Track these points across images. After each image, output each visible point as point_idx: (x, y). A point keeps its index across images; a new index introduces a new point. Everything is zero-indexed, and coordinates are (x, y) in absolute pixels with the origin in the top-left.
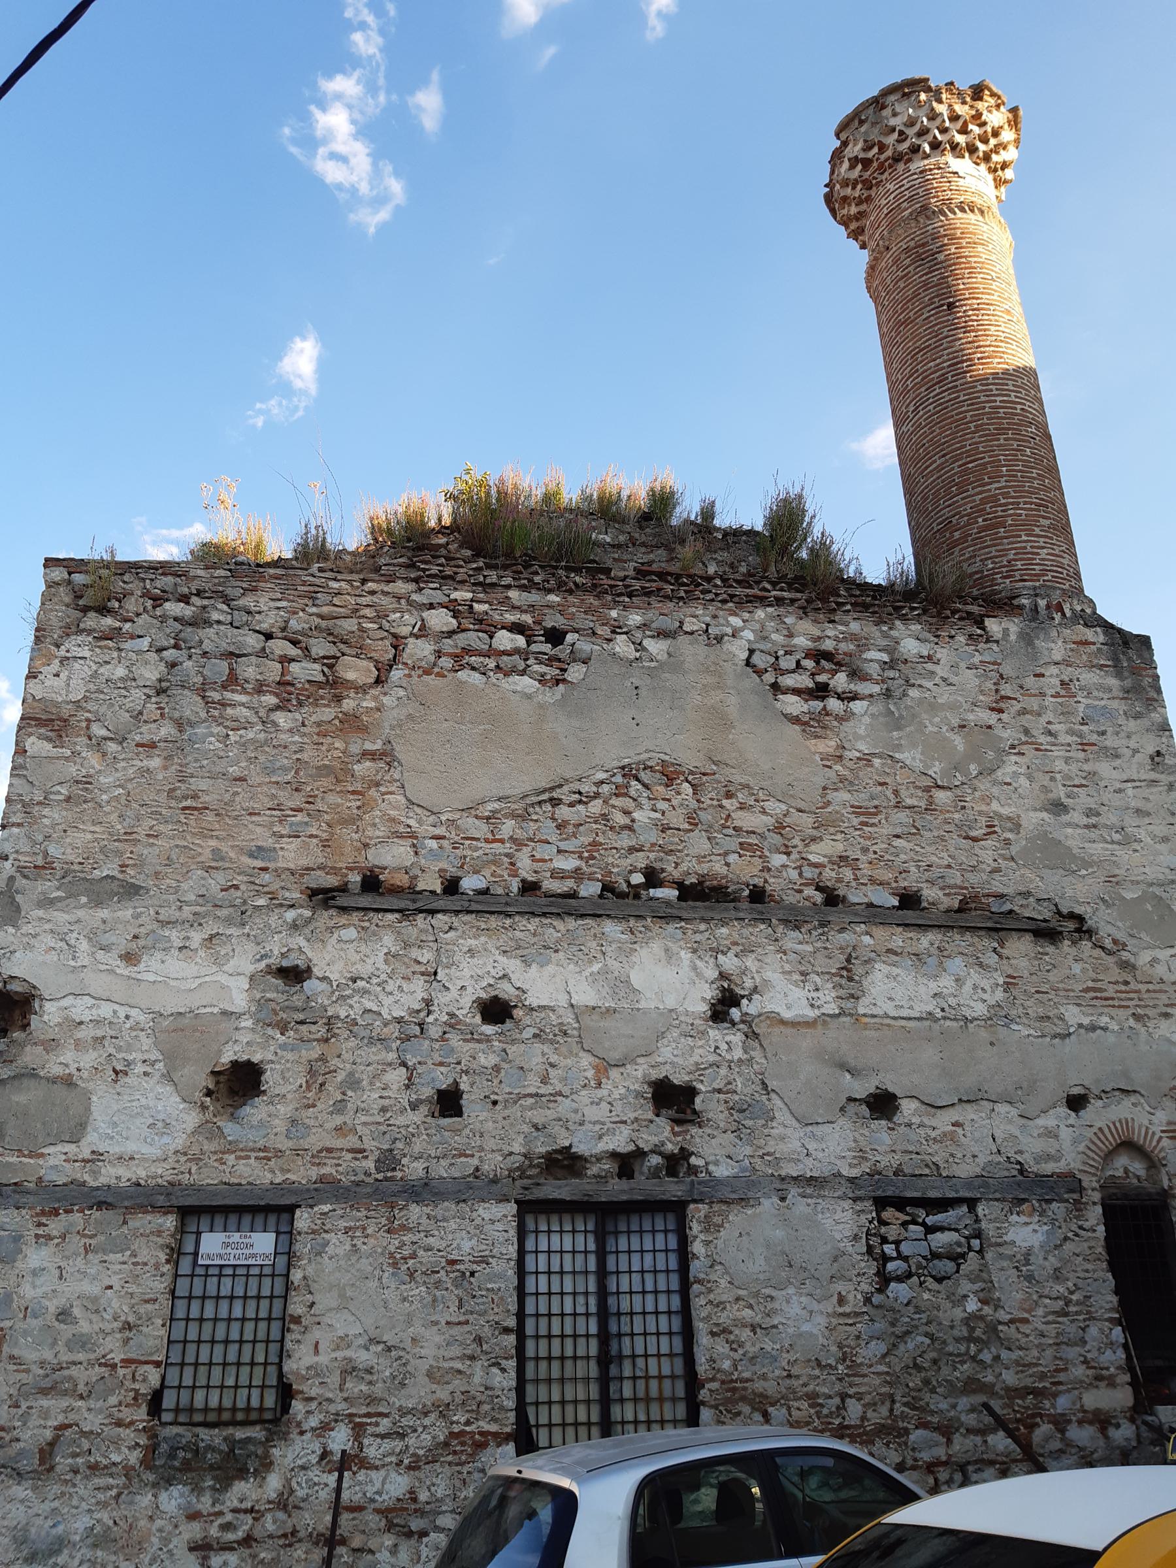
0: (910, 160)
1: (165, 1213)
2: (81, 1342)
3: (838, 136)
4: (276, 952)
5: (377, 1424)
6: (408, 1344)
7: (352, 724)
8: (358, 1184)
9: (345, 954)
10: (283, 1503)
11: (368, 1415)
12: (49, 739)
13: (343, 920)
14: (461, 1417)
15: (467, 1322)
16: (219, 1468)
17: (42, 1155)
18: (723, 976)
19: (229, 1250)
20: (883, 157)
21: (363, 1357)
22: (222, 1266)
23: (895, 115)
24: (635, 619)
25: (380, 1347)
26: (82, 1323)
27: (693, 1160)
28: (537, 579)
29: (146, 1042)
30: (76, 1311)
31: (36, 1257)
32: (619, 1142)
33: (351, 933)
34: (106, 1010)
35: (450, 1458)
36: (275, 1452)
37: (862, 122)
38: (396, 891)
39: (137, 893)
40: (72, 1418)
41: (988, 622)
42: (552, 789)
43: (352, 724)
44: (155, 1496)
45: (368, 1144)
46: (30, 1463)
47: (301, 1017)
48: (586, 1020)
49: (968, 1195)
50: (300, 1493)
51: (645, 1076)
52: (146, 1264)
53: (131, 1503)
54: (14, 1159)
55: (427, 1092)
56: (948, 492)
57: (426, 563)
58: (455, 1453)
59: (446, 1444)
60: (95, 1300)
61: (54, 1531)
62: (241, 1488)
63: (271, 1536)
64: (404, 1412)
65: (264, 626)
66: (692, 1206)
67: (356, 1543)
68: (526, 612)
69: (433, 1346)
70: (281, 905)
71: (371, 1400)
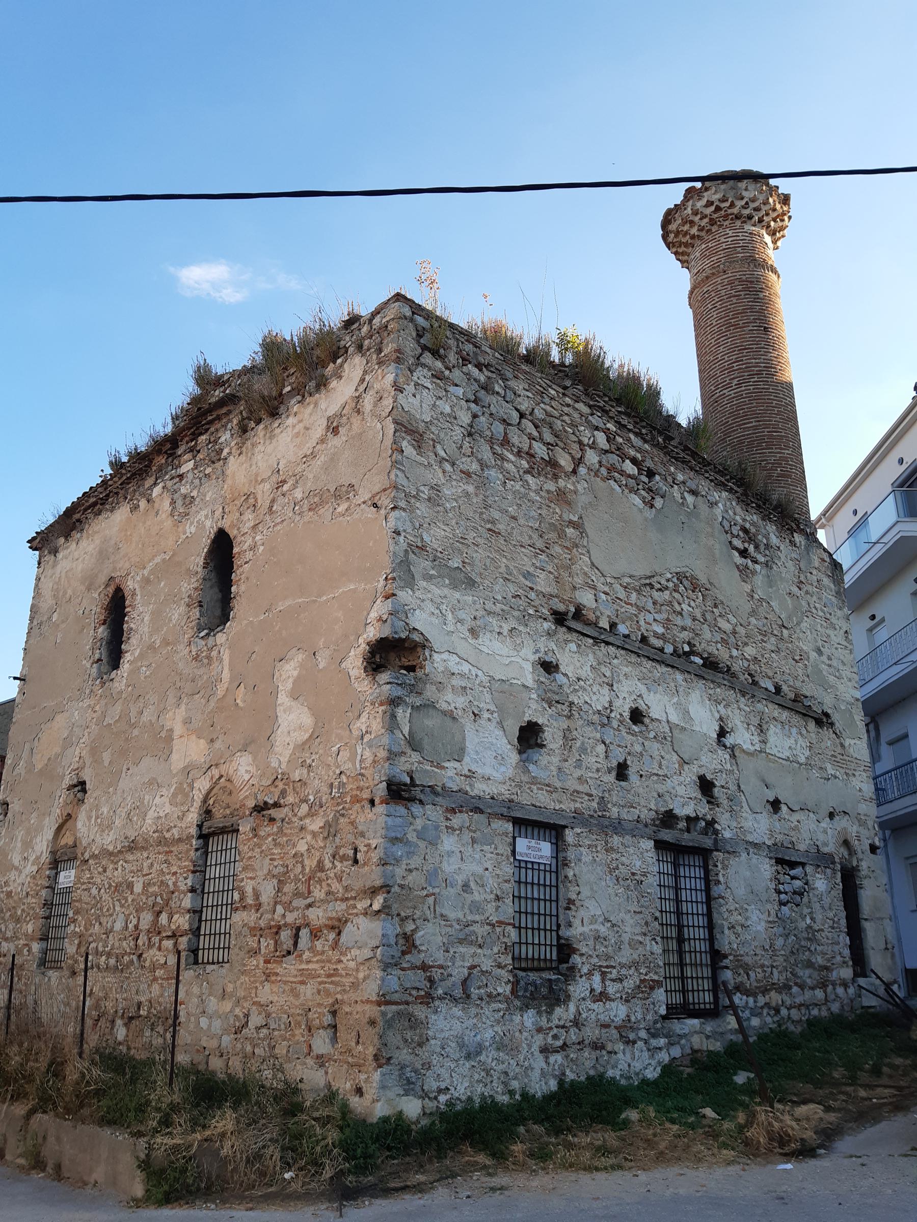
0: (745, 222)
1: (508, 821)
2: (476, 907)
6: (620, 924)
7: (561, 496)
9: (575, 659)
10: (577, 1023)
11: (607, 967)
12: (414, 448)
13: (569, 636)
14: (643, 971)
17: (443, 768)
18: (721, 719)
19: (530, 851)
20: (730, 211)
21: (603, 930)
23: (746, 190)
24: (680, 477)
25: (609, 924)
26: (476, 893)
27: (716, 826)
28: (644, 431)
30: (472, 884)
31: (448, 843)
32: (689, 811)
34: (465, 668)
35: (641, 995)
36: (571, 988)
38: (588, 623)
39: (473, 586)
40: (476, 961)
41: (795, 535)
42: (650, 577)
43: (561, 496)
45: (594, 792)
46: (458, 992)
47: (557, 698)
48: (676, 732)
51: (698, 772)
52: (502, 855)
53: (512, 1020)
54: (429, 768)
56: (759, 445)
57: (598, 396)
60: (481, 877)
62: (558, 1011)
64: (622, 966)
67: (609, 1049)
69: (631, 927)
70: (541, 617)
71: (608, 957)
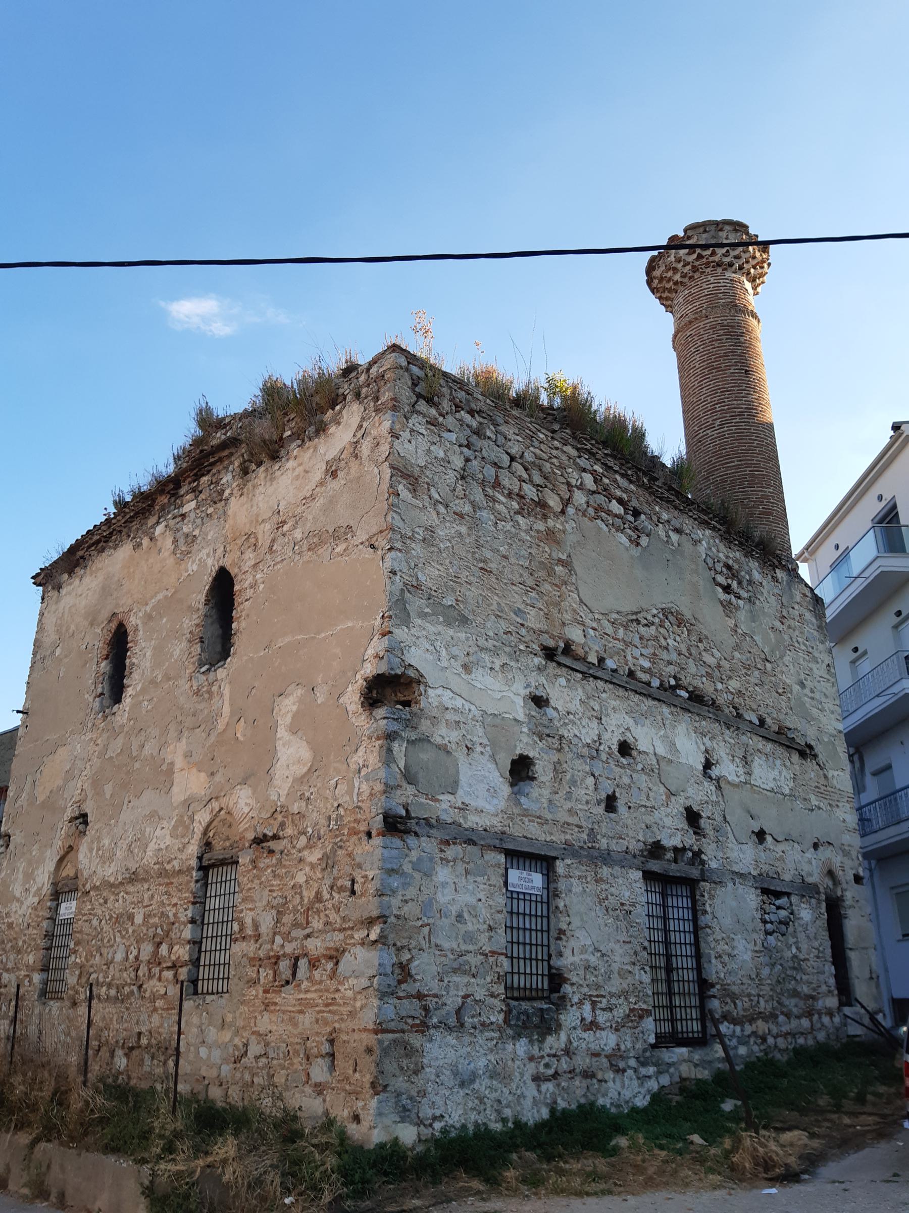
2: (469, 938)
3: (685, 231)
4: (533, 684)
5: (601, 1002)
7: (551, 536)
8: (582, 848)
10: (568, 1052)
11: (597, 996)
14: (632, 1000)
15: (630, 942)
16: (539, 1027)
17: (438, 800)
18: (707, 751)
20: (711, 259)
22: (518, 893)
24: (665, 516)
25: (599, 954)
26: (469, 924)
27: (703, 856)
28: (629, 472)
29: (480, 731)
30: (466, 915)
31: (443, 874)
33: (562, 681)
34: (459, 702)
35: (630, 1024)
37: (705, 231)
38: (577, 658)
39: (467, 623)
40: (470, 990)
42: (636, 613)
43: (551, 536)
44: (514, 1045)
45: (584, 824)
47: (547, 731)
48: (663, 765)
49: (787, 890)
50: (575, 1044)
54: (424, 801)
55: (603, 796)
57: (586, 439)
58: (632, 1021)
59: (629, 1016)
60: (475, 908)
61: (469, 1067)
62: (550, 1040)
63: (565, 1072)
64: (612, 995)
65: (513, 452)
66: (702, 883)
68: (626, 493)
69: (620, 956)
71: (598, 987)
